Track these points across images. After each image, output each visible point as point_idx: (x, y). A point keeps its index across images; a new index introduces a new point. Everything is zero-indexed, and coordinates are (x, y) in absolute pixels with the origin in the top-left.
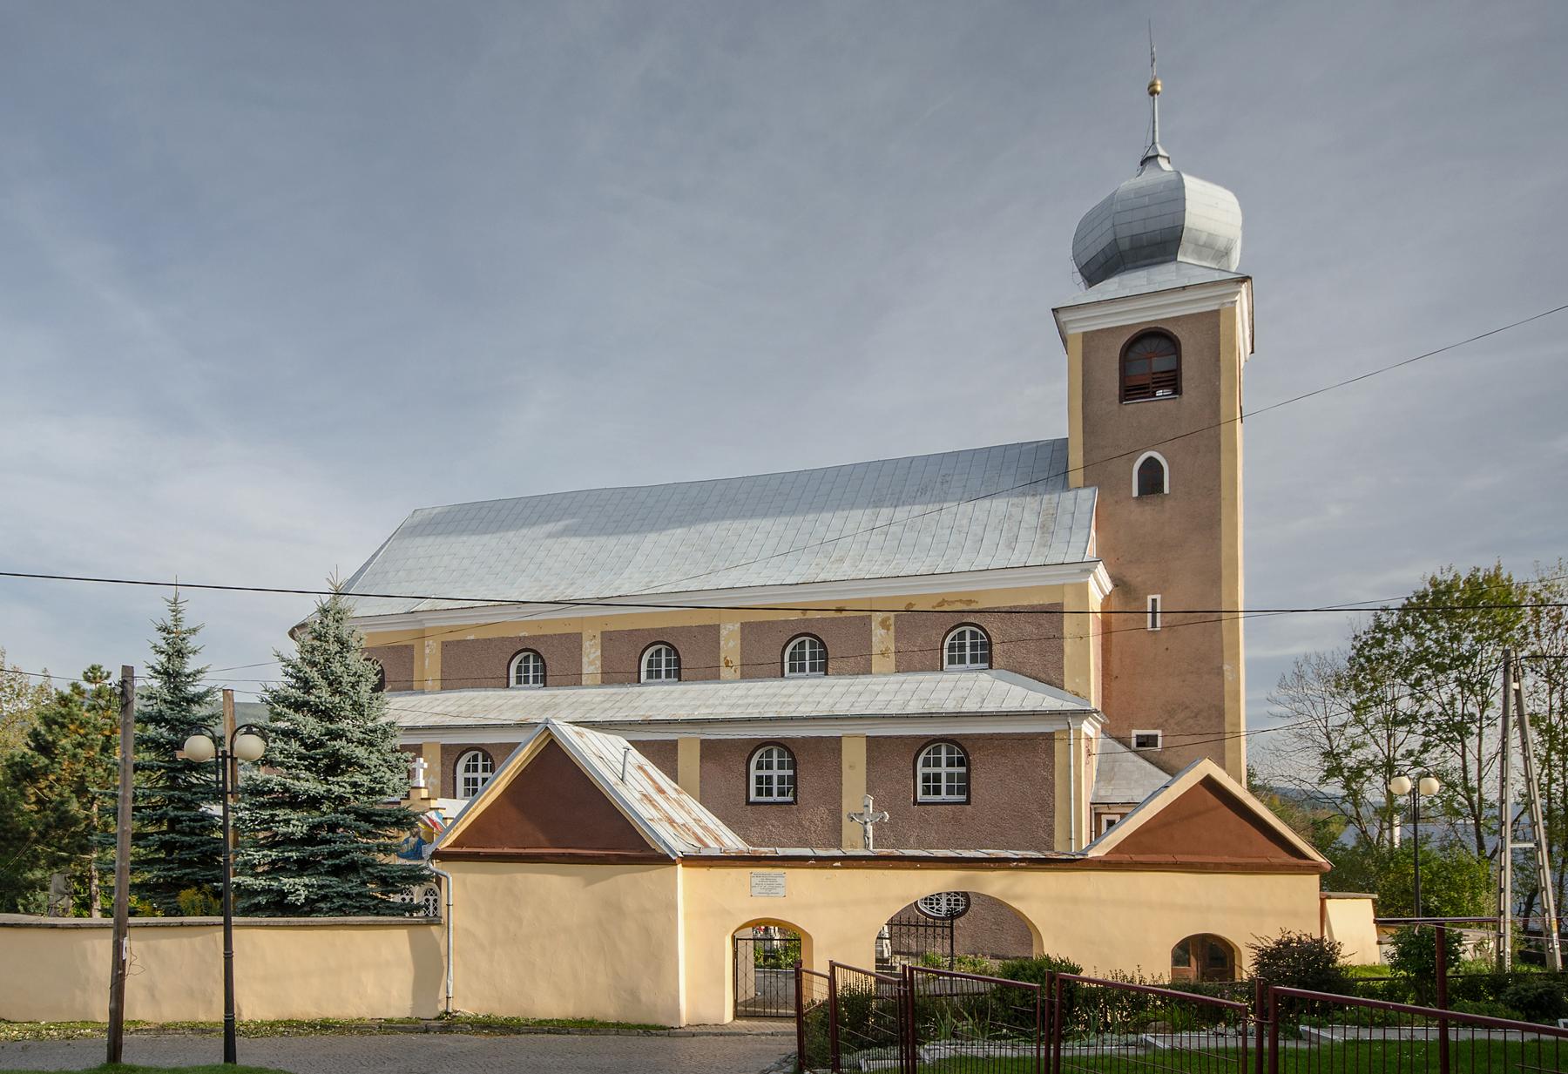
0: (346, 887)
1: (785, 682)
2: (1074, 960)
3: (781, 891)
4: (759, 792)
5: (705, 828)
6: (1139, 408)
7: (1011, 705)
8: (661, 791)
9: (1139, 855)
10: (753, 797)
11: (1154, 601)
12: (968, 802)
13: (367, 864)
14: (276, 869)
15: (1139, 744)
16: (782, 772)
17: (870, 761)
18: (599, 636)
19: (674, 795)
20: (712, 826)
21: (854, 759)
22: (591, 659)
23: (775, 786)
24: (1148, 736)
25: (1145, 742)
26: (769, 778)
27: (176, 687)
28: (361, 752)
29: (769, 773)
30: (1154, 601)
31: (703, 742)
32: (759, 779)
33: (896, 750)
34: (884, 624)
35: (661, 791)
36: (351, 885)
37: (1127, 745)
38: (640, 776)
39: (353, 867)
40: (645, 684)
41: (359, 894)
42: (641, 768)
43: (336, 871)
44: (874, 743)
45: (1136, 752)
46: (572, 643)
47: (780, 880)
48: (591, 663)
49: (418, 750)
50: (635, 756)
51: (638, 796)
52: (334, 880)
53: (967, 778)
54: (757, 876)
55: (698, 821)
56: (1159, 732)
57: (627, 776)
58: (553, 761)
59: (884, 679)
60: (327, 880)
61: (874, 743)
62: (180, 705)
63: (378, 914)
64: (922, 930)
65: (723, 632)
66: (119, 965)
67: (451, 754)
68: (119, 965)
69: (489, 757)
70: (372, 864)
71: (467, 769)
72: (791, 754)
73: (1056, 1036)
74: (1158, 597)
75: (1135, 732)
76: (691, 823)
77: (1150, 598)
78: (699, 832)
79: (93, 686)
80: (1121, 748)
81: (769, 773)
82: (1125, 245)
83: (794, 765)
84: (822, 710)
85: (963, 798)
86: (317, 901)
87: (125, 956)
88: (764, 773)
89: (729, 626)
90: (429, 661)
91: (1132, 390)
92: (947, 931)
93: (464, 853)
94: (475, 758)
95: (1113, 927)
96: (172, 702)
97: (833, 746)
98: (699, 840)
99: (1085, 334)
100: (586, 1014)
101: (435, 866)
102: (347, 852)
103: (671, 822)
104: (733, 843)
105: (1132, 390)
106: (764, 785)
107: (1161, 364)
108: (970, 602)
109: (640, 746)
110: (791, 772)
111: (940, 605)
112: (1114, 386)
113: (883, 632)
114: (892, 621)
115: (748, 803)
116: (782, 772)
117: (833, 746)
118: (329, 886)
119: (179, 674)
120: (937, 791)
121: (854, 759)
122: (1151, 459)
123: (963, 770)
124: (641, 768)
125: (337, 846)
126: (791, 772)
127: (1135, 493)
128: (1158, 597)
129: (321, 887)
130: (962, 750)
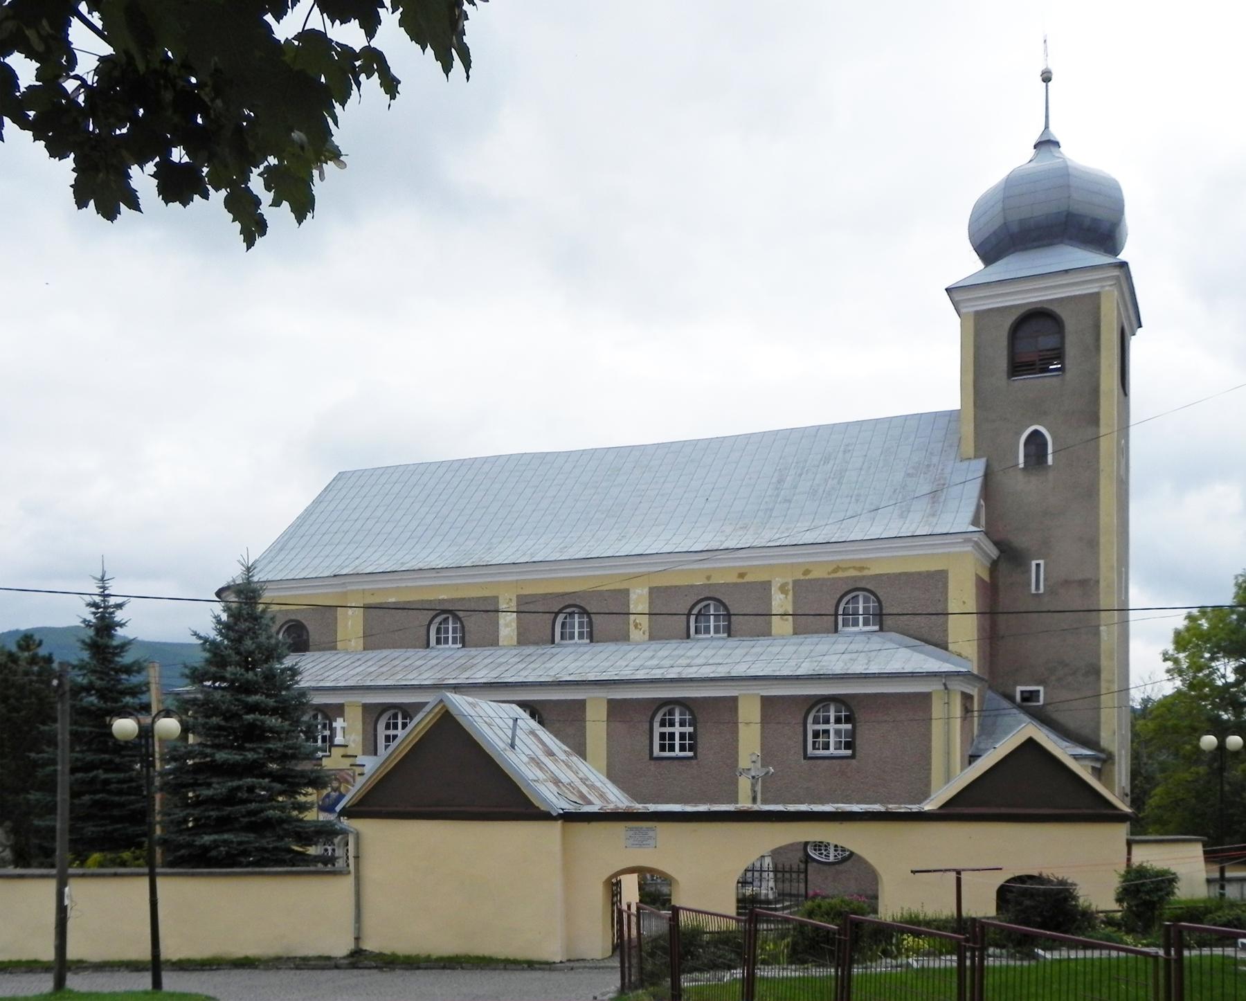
0: (264, 842)
1: (690, 644)
2: (996, 888)
3: (652, 842)
4: (662, 748)
5: (592, 787)
6: (1030, 383)
7: (895, 666)
8: (550, 754)
9: (962, 809)
10: (657, 752)
11: (1038, 565)
12: (853, 757)
13: (281, 821)
14: (201, 828)
15: (1024, 699)
16: (683, 729)
17: (765, 720)
18: (514, 599)
19: (563, 757)
20: (598, 784)
21: (749, 713)
22: (508, 626)
23: (677, 742)
24: (1031, 692)
25: (1029, 697)
26: (672, 735)
27: (105, 659)
28: (273, 721)
29: (671, 730)
30: (1038, 565)
31: (610, 701)
32: (662, 736)
33: (793, 709)
34: (783, 589)
35: (550, 754)
36: (268, 842)
37: (1011, 698)
38: (530, 741)
39: (269, 824)
40: (559, 645)
41: (275, 848)
42: (533, 733)
43: (253, 827)
44: (767, 702)
45: (1020, 707)
46: (490, 609)
47: (651, 833)
48: (507, 626)
49: (339, 710)
50: (524, 715)
51: (525, 759)
52: (252, 836)
53: (853, 734)
54: (631, 829)
55: (584, 780)
56: (1041, 688)
57: (517, 741)
58: (448, 727)
59: (783, 642)
60: (243, 837)
61: (767, 702)
62: (108, 674)
63: (293, 865)
64: (794, 875)
65: (633, 596)
66: (62, 911)
67: (373, 713)
68: (62, 911)
69: (407, 711)
70: (290, 820)
71: (388, 727)
72: (692, 713)
73: (845, 964)
74: (1041, 562)
75: (1019, 689)
76: (578, 783)
77: (1034, 563)
78: (584, 790)
79: (26, 654)
80: (1005, 704)
81: (671, 730)
82: (1015, 228)
83: (693, 723)
84: (721, 672)
85: (849, 752)
86: (238, 855)
87: (67, 902)
88: (667, 730)
89: (639, 591)
90: (351, 624)
91: (1017, 367)
92: (802, 876)
93: (366, 808)
94: (395, 716)
95: (930, 873)
96: (101, 672)
97: (731, 704)
98: (583, 796)
99: (977, 313)
100: (135, 975)
101: (346, 822)
102: (262, 811)
103: (557, 782)
104: (617, 799)
105: (1017, 367)
106: (667, 741)
107: (1047, 342)
108: (862, 569)
109: (533, 710)
110: (691, 729)
111: (835, 571)
112: (1003, 363)
113: (782, 596)
114: (790, 587)
115: (652, 758)
116: (683, 729)
117: (731, 704)
118: (248, 842)
119: (107, 647)
120: (672, 748)
121: (749, 713)
122: (1036, 432)
123: (849, 726)
124: (533, 733)
125: (253, 806)
126: (691, 729)
127: (1022, 466)
128: (1041, 562)
129: (240, 843)
130: (850, 708)
